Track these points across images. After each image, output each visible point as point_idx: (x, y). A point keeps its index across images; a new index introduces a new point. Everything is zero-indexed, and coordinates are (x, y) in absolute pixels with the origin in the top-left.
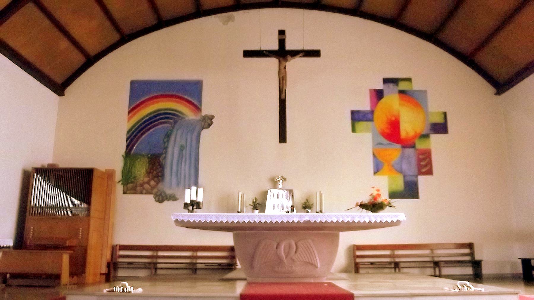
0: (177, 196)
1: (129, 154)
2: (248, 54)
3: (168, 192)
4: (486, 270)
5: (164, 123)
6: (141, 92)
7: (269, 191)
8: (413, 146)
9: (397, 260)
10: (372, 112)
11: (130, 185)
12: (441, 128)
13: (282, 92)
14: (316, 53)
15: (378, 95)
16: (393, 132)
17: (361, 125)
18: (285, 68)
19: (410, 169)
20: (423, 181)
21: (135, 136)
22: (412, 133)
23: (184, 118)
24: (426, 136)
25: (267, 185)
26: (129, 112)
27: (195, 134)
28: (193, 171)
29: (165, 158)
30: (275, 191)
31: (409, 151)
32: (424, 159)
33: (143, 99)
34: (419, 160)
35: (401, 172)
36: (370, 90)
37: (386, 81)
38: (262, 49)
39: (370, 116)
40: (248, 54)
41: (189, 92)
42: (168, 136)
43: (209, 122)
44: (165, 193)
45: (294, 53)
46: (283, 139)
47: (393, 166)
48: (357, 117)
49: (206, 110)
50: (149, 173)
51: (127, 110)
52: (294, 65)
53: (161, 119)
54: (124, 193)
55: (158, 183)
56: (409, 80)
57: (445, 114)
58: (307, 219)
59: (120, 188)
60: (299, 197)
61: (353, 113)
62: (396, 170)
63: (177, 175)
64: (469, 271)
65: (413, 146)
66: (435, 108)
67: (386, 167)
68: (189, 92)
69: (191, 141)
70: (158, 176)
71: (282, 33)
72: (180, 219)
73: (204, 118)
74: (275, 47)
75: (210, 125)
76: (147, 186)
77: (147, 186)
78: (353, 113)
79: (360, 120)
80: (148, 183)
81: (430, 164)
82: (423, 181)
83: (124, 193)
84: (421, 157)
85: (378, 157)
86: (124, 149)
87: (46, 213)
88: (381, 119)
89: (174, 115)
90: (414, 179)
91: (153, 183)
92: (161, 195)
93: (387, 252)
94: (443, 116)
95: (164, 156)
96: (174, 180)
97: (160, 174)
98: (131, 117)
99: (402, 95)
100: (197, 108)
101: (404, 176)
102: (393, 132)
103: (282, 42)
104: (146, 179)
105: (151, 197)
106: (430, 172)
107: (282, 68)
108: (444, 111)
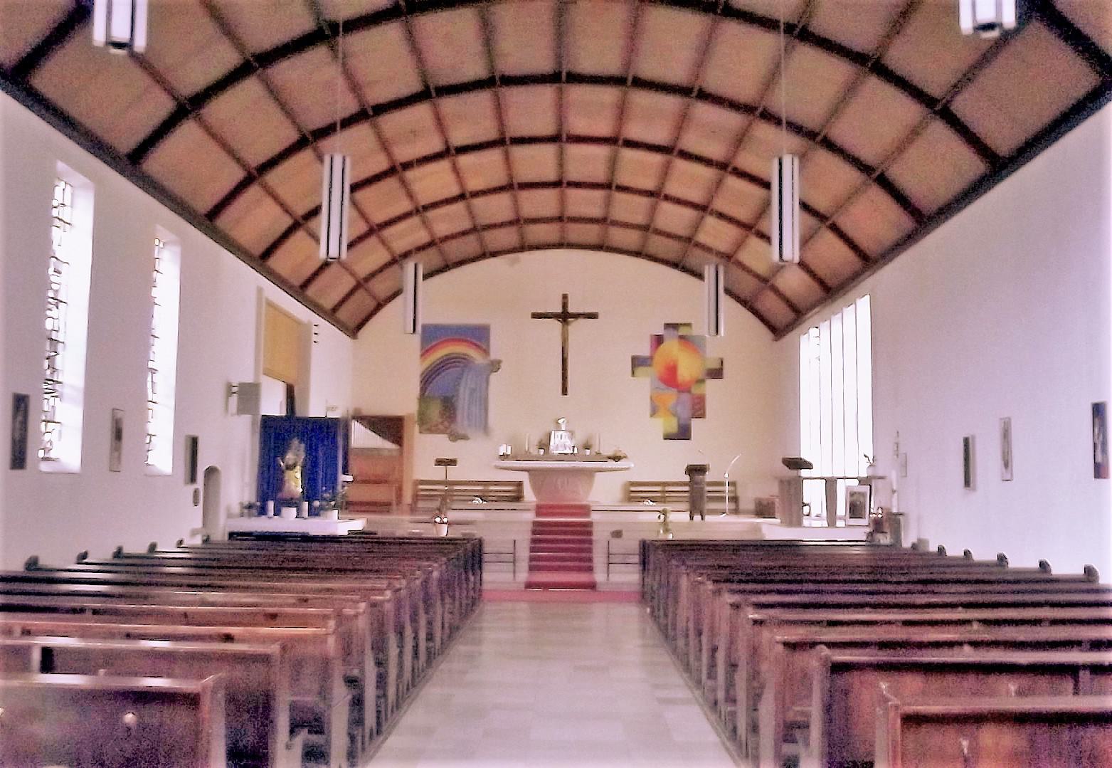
0: (469, 436)
1: (423, 398)
2: (535, 316)
3: (461, 432)
6: (432, 336)
7: (553, 432)
8: (689, 391)
9: (842, 509)
10: (651, 358)
11: (425, 427)
12: (717, 373)
13: (564, 361)
15: (659, 340)
16: (670, 377)
17: (640, 370)
19: (685, 411)
20: (695, 424)
24: (701, 381)
25: (552, 427)
26: (422, 355)
30: (559, 433)
31: (685, 397)
33: (434, 343)
34: (694, 405)
35: (675, 415)
36: (651, 336)
37: (668, 326)
40: (535, 316)
41: (478, 336)
42: (459, 378)
45: (577, 316)
47: (669, 410)
48: (637, 362)
50: (442, 415)
51: (419, 353)
52: (576, 326)
54: (420, 432)
56: (689, 325)
59: (417, 428)
60: (580, 437)
62: (672, 414)
64: (727, 505)
66: (713, 352)
68: (478, 336)
70: (450, 417)
71: (565, 297)
74: (559, 310)
77: (441, 427)
79: (639, 365)
82: (695, 424)
89: (464, 359)
98: (423, 361)
99: (683, 341)
100: (486, 352)
102: (670, 377)
103: (565, 305)
108: (721, 356)
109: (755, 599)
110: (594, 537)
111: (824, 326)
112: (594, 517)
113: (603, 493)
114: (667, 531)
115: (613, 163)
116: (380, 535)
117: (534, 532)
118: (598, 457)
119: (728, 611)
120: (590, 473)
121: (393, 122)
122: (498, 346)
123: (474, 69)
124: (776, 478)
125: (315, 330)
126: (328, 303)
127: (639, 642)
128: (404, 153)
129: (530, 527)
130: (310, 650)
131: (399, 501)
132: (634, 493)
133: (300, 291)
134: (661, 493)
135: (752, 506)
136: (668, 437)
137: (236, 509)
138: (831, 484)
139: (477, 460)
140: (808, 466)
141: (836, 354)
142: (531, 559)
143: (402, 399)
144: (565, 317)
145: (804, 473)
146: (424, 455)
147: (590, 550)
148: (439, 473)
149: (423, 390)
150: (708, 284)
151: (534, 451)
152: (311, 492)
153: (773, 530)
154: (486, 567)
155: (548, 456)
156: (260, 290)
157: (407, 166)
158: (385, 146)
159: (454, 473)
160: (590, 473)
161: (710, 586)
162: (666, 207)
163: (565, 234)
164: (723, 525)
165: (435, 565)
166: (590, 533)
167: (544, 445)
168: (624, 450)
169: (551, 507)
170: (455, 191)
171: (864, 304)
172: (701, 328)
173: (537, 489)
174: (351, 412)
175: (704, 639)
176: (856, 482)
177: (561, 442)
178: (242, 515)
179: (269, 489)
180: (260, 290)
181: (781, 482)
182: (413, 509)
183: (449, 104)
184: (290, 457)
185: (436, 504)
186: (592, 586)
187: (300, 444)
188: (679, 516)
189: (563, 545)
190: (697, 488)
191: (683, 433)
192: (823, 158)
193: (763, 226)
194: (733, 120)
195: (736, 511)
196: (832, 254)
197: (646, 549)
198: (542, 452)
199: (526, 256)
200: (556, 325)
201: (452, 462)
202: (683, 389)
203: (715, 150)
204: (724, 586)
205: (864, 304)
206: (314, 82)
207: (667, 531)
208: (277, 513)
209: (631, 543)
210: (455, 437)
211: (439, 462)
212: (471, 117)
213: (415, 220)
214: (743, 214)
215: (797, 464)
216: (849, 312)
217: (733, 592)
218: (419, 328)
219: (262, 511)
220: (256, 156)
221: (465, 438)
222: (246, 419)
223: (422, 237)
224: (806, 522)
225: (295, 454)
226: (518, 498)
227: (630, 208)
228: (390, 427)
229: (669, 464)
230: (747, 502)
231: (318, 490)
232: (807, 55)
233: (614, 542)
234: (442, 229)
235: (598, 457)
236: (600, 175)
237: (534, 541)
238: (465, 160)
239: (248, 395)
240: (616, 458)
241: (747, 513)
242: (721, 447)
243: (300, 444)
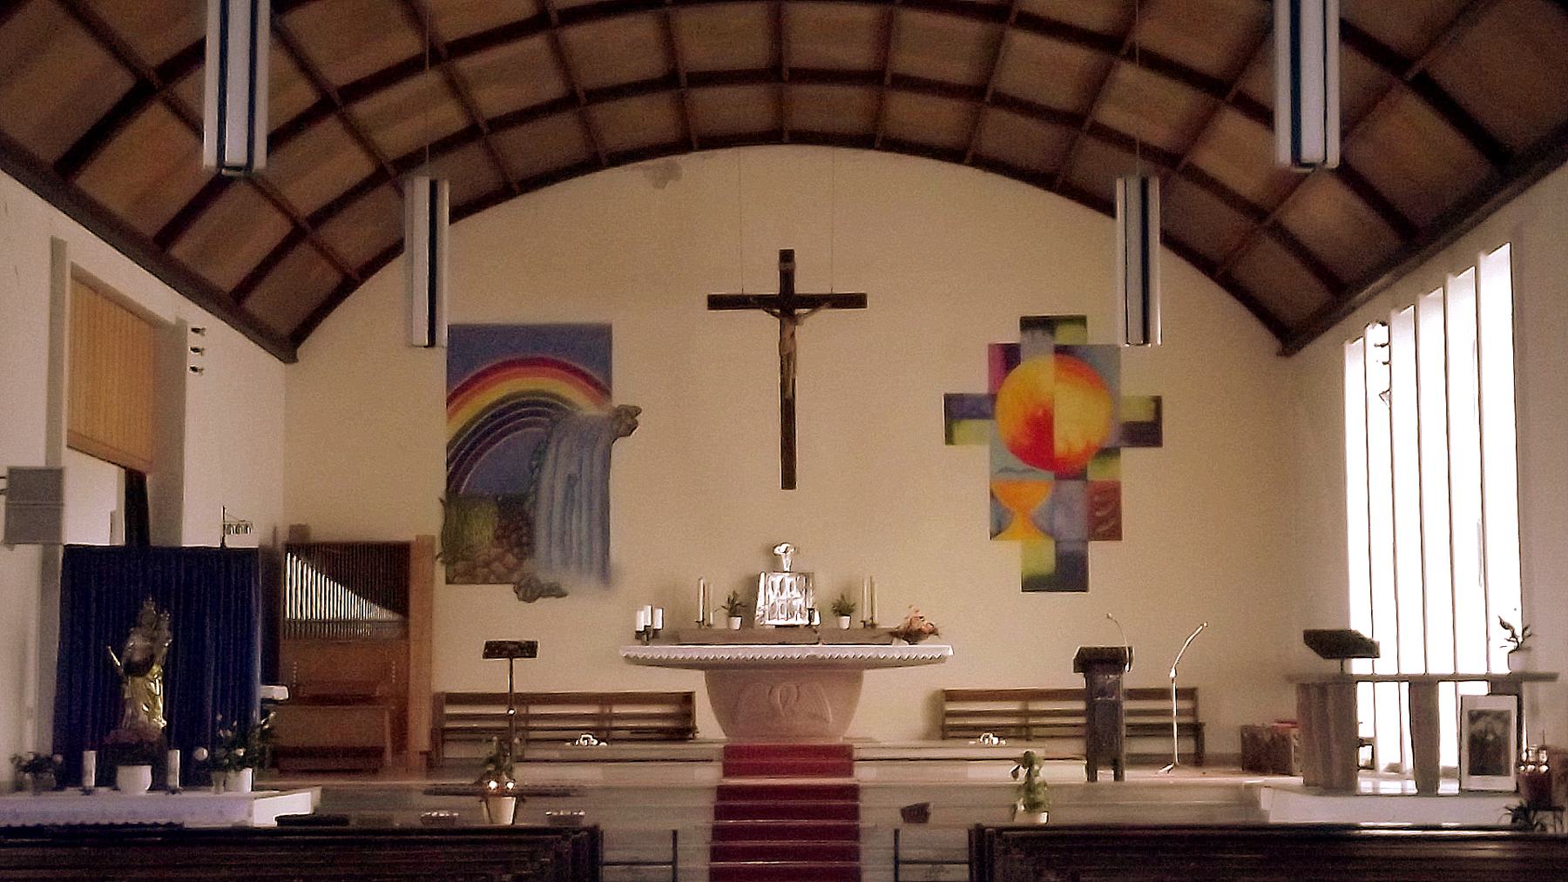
1: (454, 498)
2: (716, 302)
3: (545, 578)
4: (1212, 746)
5: (530, 424)
6: (474, 354)
8: (1080, 475)
10: (993, 397)
11: (460, 566)
12: (1146, 433)
14: (857, 301)
15: (1008, 357)
16: (1036, 443)
17: (966, 428)
18: (793, 335)
19: (1071, 525)
20: (1099, 554)
21: (467, 453)
22: (1079, 446)
23: (569, 413)
24: (1108, 453)
26: (449, 401)
27: (601, 446)
28: (597, 531)
29: (534, 504)
30: (777, 579)
31: (1072, 488)
32: (1104, 505)
34: (1094, 506)
35: (1051, 533)
36: (992, 347)
37: (1028, 324)
38: (747, 292)
39: (985, 407)
40: (716, 302)
42: (539, 452)
43: (629, 421)
44: (537, 581)
45: (814, 302)
46: (789, 481)
48: (958, 409)
49: (622, 395)
52: (814, 328)
53: (521, 415)
54: (448, 582)
55: (521, 559)
56: (1081, 321)
57: (1158, 401)
58: (812, 653)
59: (440, 572)
60: (827, 588)
61: (949, 399)
62: (1044, 531)
63: (562, 541)
65: (1080, 475)
66: (1137, 381)
67: (1017, 524)
68: (585, 352)
69: (592, 465)
70: (520, 544)
71: (787, 257)
72: (632, 654)
74: (773, 288)
75: (631, 429)
76: (496, 566)
77: (496, 566)
78: (949, 399)
79: (963, 416)
80: (500, 558)
81: (1116, 514)
82: (1099, 554)
83: (448, 582)
84: (1096, 498)
85: (998, 495)
86: (444, 487)
90: (1081, 547)
91: (511, 559)
92: (528, 585)
93: (1014, 706)
94: (1153, 405)
95: (532, 499)
96: (556, 554)
97: (525, 539)
100: (603, 389)
101: (1057, 543)
102: (1036, 443)
103: (787, 277)
104: (495, 551)
106: (1115, 534)
107: (787, 335)
114: (1033, 806)
120: (850, 672)
136: (1032, 584)
143: (403, 499)
144: (787, 304)
149: (453, 480)
151: (717, 620)
155: (751, 633)
160: (850, 672)
167: (741, 606)
180: (57, 248)
184: (137, 643)
191: (1069, 575)
198: (736, 622)
199: (692, 164)
200: (766, 324)
202: (1067, 470)
221: (556, 592)
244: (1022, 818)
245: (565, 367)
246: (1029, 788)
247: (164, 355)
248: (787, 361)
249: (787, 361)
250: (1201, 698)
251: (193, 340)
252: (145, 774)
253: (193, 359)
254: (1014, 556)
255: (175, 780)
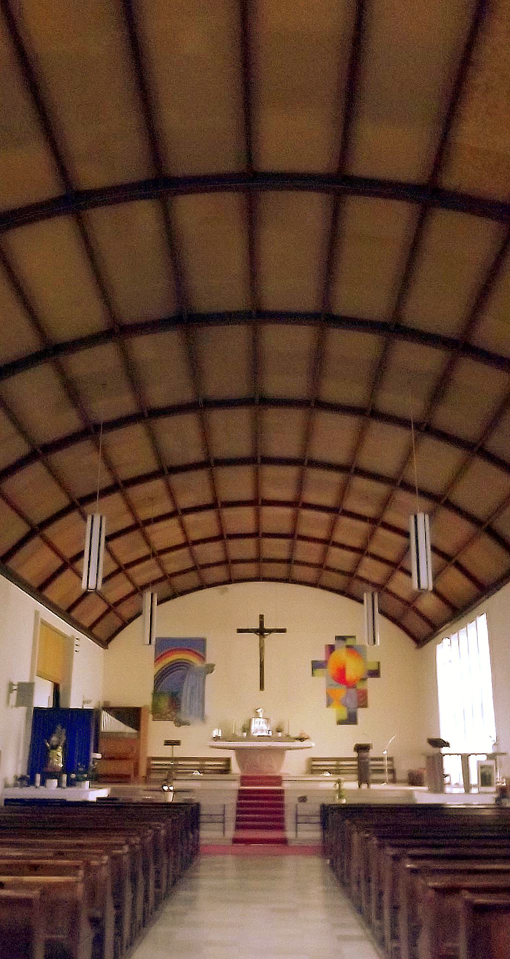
1: (156, 694)
2: (240, 631)
3: (184, 719)
4: (399, 776)
6: (164, 646)
8: (354, 687)
9: (474, 779)
10: (326, 662)
12: (375, 673)
14: (284, 631)
15: (331, 649)
16: (341, 677)
17: (318, 671)
19: (352, 703)
20: (361, 712)
22: (354, 677)
24: (364, 680)
30: (258, 720)
31: (352, 691)
34: (359, 697)
35: (345, 705)
37: (338, 638)
40: (240, 631)
41: (197, 646)
42: (183, 678)
45: (270, 631)
49: (209, 660)
52: (270, 639)
56: (354, 637)
59: (151, 716)
60: (274, 723)
64: (387, 776)
65: (354, 687)
66: (373, 656)
68: (197, 646)
71: (262, 617)
73: (208, 666)
74: (257, 627)
77: (169, 715)
82: (361, 712)
87: (114, 737)
88: (331, 669)
100: (203, 658)
102: (341, 677)
103: (262, 623)
105: (171, 724)
109: (393, 842)
110: (286, 802)
111: (454, 637)
112: (286, 786)
113: (291, 767)
114: (341, 797)
115: (295, 519)
116: (121, 801)
117: (240, 798)
118: (288, 738)
119: (390, 862)
121: (138, 492)
122: (212, 655)
123: (195, 455)
124: (423, 754)
125: (76, 642)
126: (87, 623)
127: (321, 888)
128: (145, 513)
129: (235, 795)
130: (65, 895)
131: (136, 772)
132: (314, 767)
133: (67, 613)
134: (337, 768)
135: (405, 777)
136: (340, 722)
137: (11, 781)
138: (465, 758)
139: (196, 741)
140: (447, 745)
141: (464, 657)
142: (238, 819)
143: (140, 694)
144: (261, 631)
145: (444, 750)
146: (157, 738)
147: (282, 813)
148: (167, 752)
150: (366, 607)
151: (239, 734)
152: (69, 767)
153: (423, 796)
154: (203, 826)
155: (249, 738)
156: (37, 613)
157: (148, 522)
158: (131, 509)
159: (178, 752)
160: (281, 751)
161: (375, 841)
162: (335, 551)
163: (262, 570)
164: (385, 792)
165: (163, 825)
166: (282, 799)
167: (247, 729)
168: (307, 733)
169: (259, 778)
170: (180, 540)
171: (482, 620)
172: (362, 639)
173: (241, 764)
174: (102, 705)
175: (373, 886)
176: (484, 758)
177: (259, 727)
178: (15, 785)
179: (37, 765)
180: (37, 613)
181: (428, 757)
182: (146, 780)
183: (177, 480)
184: (54, 739)
185: (164, 776)
186: (284, 841)
187: (62, 731)
188: (350, 785)
189: (261, 809)
190: (363, 764)
191: (351, 719)
192: (446, 515)
193: (405, 564)
194: (381, 489)
195: (394, 781)
196: (456, 583)
197: (326, 812)
198: (245, 734)
200: (256, 637)
201: (177, 743)
203: (368, 510)
204: (387, 841)
205: (482, 620)
206: (83, 466)
207: (341, 797)
208: (43, 783)
209: (312, 807)
210: (179, 723)
211: (168, 743)
212: (193, 489)
213: (152, 561)
214: (391, 555)
215: (438, 743)
216: (471, 627)
217: (393, 846)
218: (153, 640)
219: (31, 782)
220: (38, 517)
222: (23, 710)
223: (157, 573)
224: (448, 789)
225: (58, 738)
226: (226, 770)
227: (308, 552)
228: (131, 716)
229: (339, 743)
230: (401, 774)
231: (76, 767)
232: (430, 444)
233: (301, 805)
234: (171, 568)
235: (288, 738)
236: (286, 528)
237: (239, 805)
238: (189, 519)
239: (25, 691)
240: (301, 739)
241: (402, 782)
242: (381, 730)
243: (62, 731)
244: (337, 801)
245: (196, 653)
246: (339, 791)
247: (68, 645)
248: (262, 649)
249: (262, 649)
250: (395, 759)
251: (76, 642)
252: (55, 782)
253: (76, 648)
254: (336, 712)
255: (64, 785)
